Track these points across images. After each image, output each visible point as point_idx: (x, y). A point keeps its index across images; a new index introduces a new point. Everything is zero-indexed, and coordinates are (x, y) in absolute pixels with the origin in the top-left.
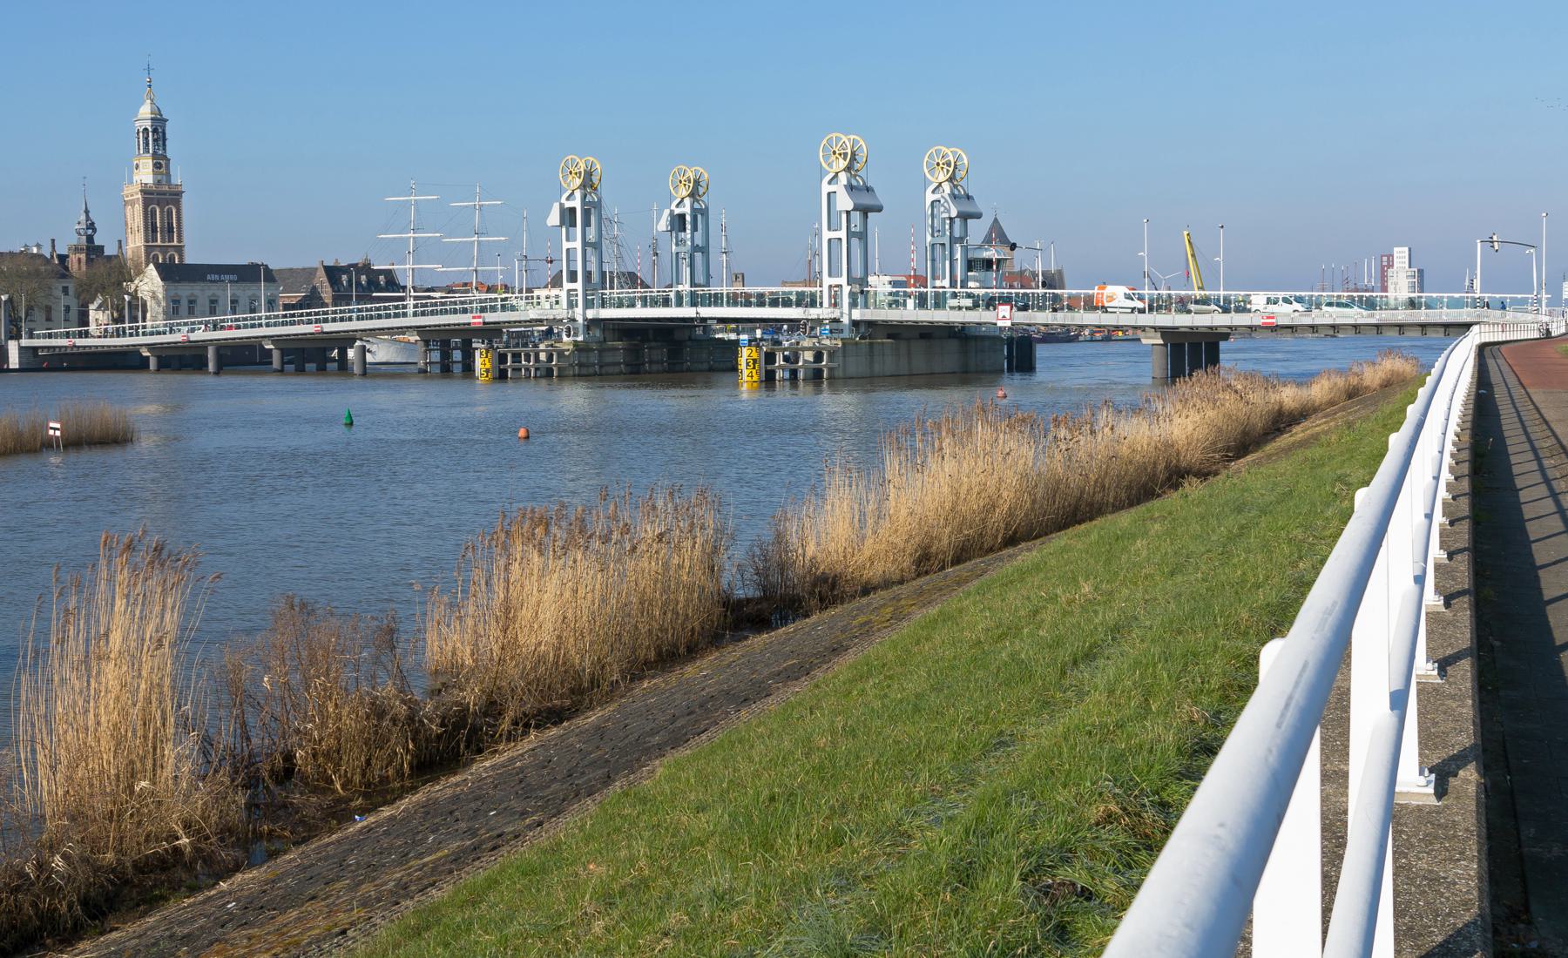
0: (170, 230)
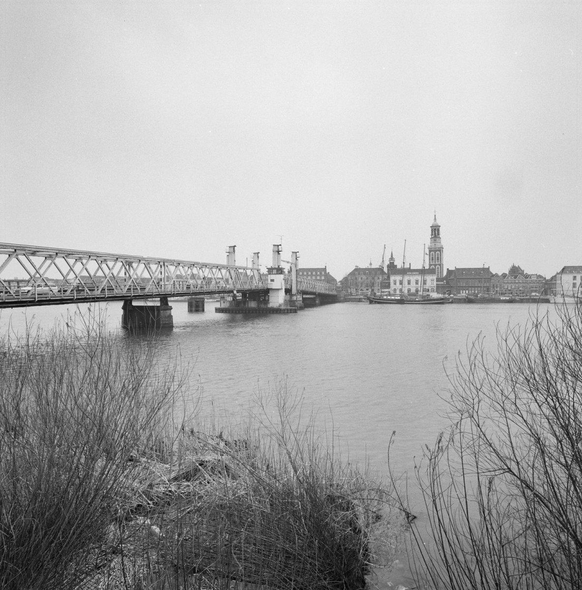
0: (438, 259)
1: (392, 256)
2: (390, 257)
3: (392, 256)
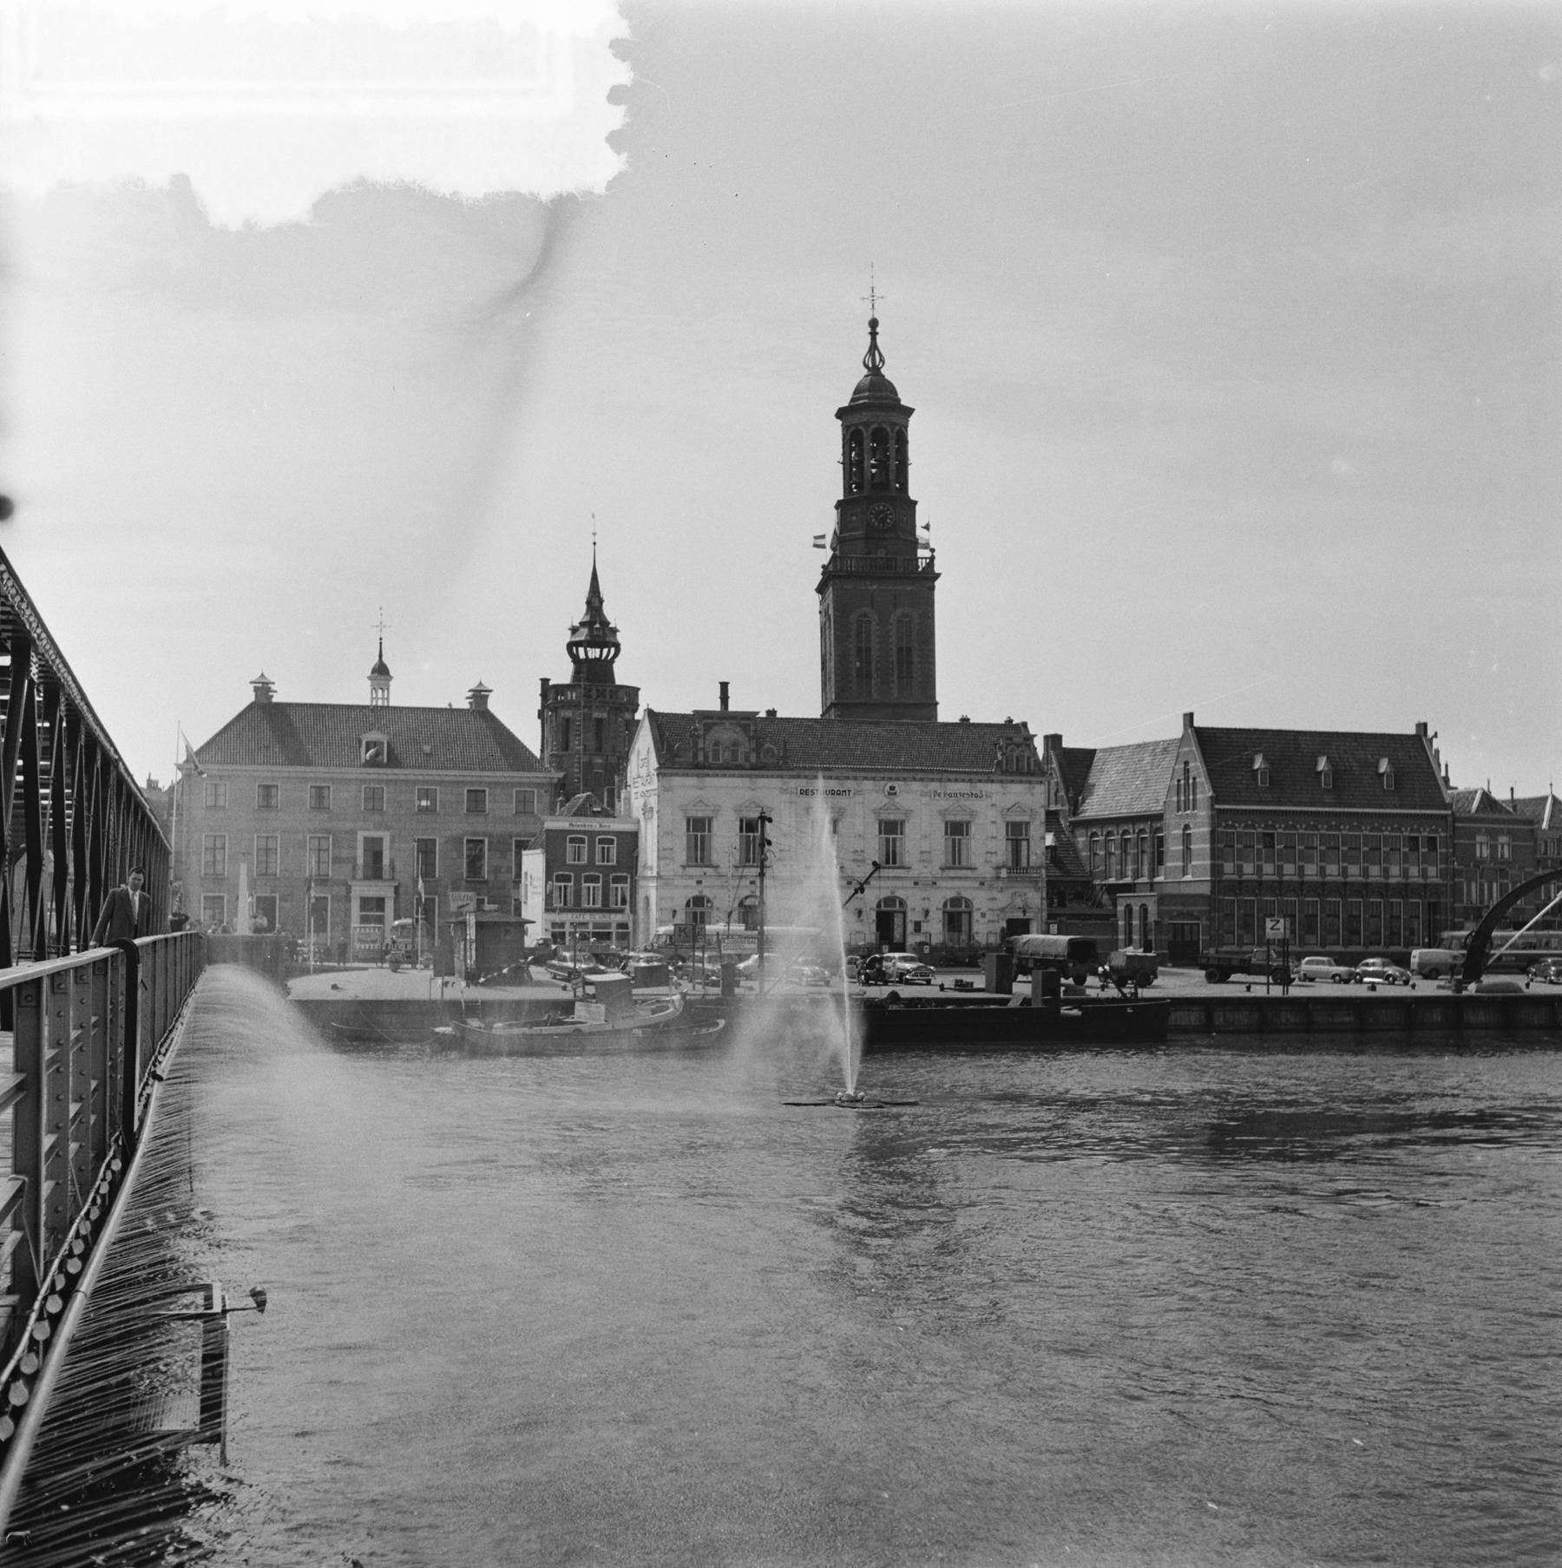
1: (595, 601)
2: (579, 613)
3: (595, 601)
